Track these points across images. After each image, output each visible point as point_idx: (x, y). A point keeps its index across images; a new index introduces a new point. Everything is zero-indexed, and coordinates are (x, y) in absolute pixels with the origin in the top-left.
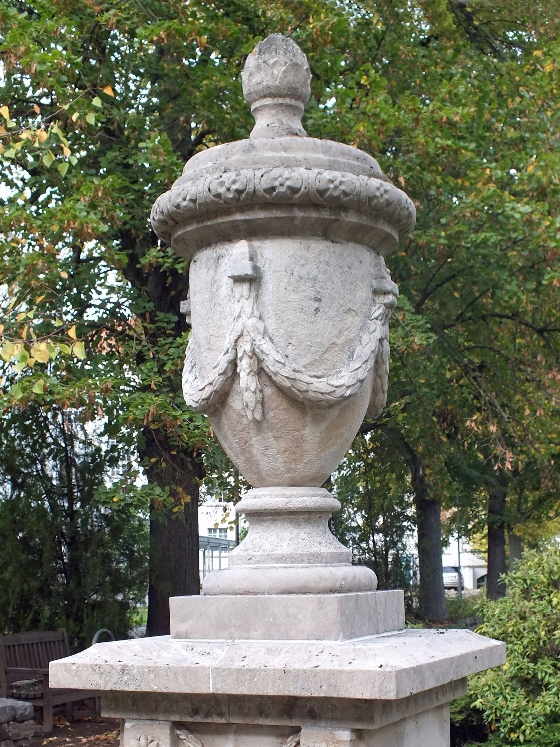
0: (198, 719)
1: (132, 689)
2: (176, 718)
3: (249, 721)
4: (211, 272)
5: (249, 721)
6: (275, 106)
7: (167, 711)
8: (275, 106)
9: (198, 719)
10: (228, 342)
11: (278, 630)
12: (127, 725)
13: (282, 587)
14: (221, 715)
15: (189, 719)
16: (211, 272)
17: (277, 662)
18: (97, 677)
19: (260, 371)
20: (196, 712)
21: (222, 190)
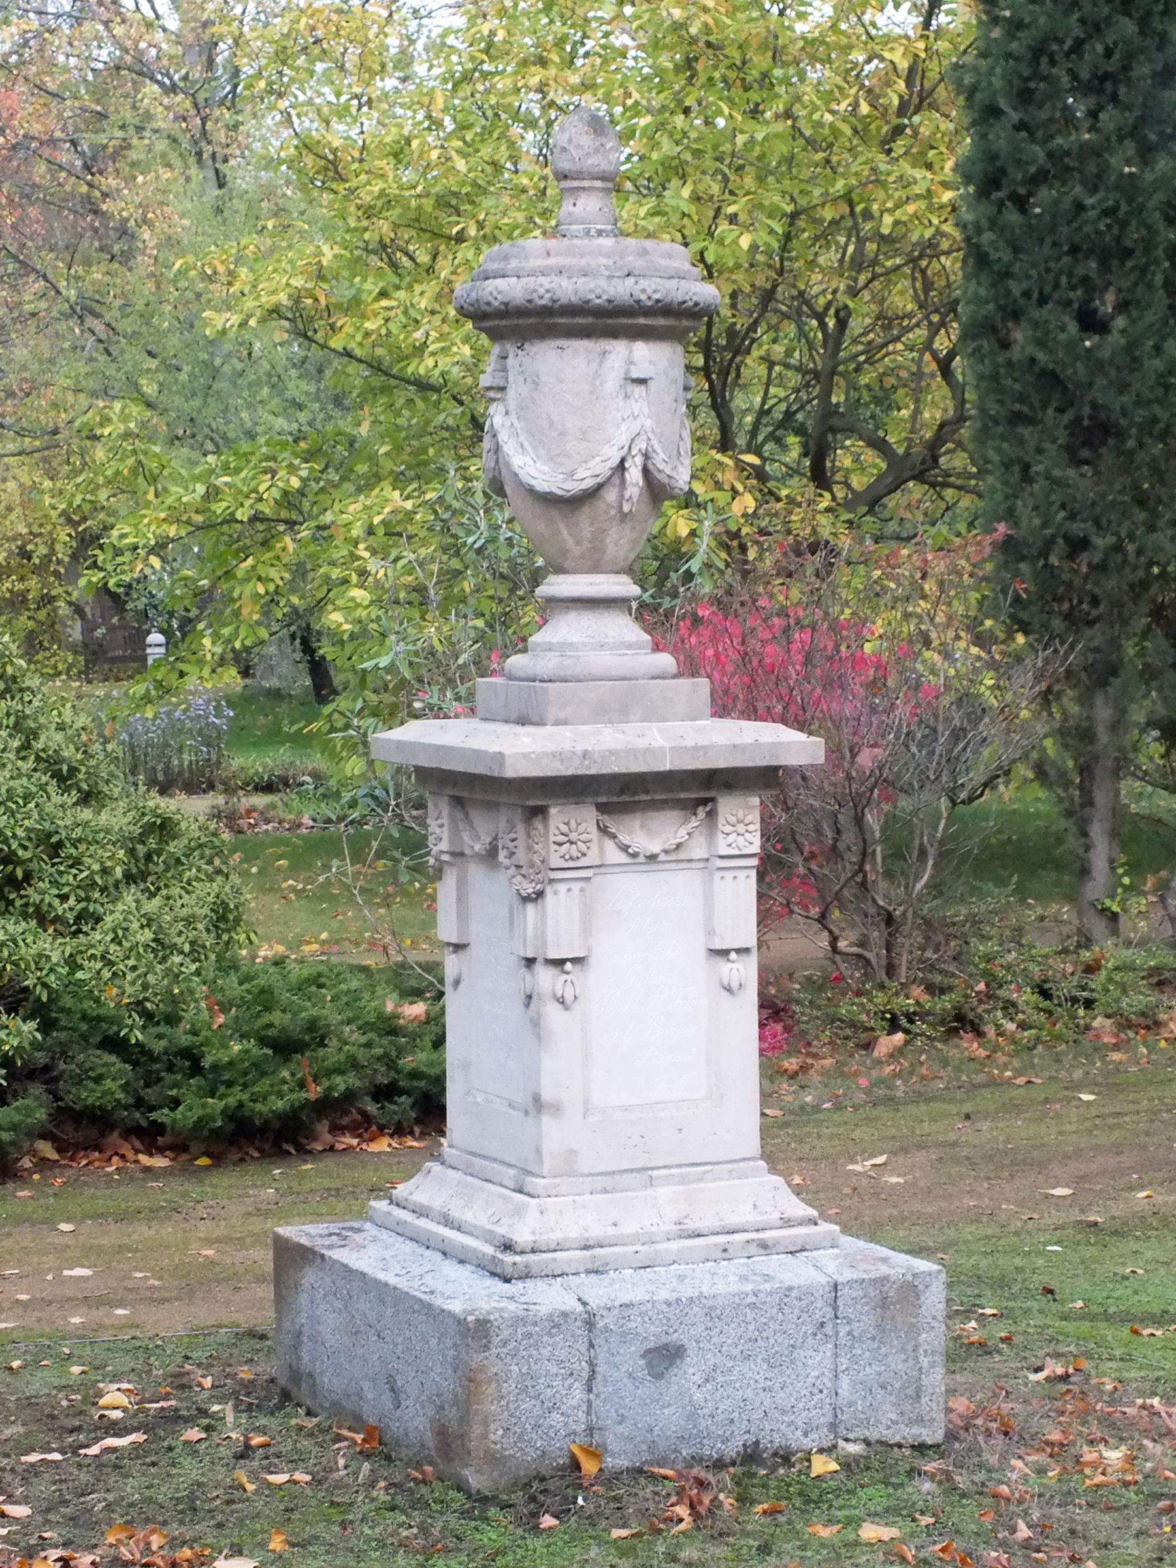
0: (625, 798)
1: (593, 772)
2: (603, 799)
3: (671, 796)
4: (594, 365)
5: (671, 796)
6: (603, 190)
7: (596, 793)
8: (603, 190)
9: (625, 798)
10: (624, 439)
11: (654, 714)
12: (553, 811)
13: (653, 672)
14: (647, 792)
15: (615, 799)
16: (594, 365)
17: (474, 744)
18: (558, 764)
19: (646, 471)
20: (622, 792)
21: (643, 297)
